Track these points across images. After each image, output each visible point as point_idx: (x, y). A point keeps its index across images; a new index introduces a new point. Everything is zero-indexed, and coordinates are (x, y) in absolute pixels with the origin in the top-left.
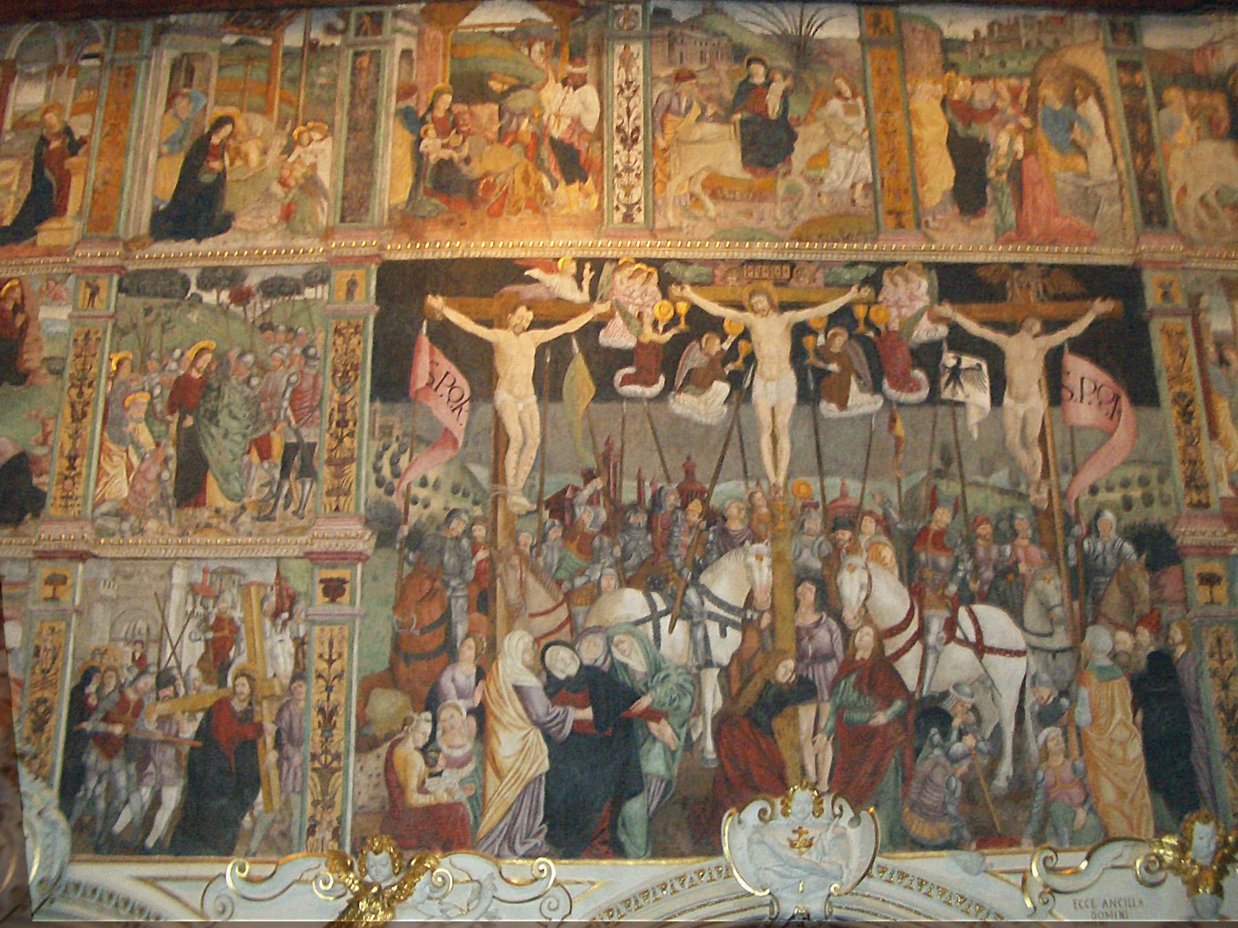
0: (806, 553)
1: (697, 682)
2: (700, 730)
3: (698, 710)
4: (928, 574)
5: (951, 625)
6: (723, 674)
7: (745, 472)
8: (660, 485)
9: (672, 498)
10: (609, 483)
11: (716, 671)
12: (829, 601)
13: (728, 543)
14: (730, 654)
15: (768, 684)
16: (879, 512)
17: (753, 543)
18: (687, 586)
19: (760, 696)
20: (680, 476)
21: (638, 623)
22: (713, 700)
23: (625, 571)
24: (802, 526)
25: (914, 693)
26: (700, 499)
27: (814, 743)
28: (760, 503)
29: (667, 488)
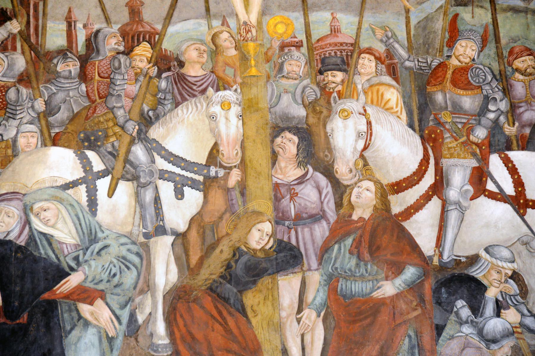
0: (286, 99)
1: (145, 253)
2: (148, 310)
3: (148, 287)
4: (446, 118)
5: (479, 177)
6: (180, 241)
7: (208, 10)
8: (96, 27)
9: (113, 41)
10: (28, 23)
11: (169, 239)
12: (314, 152)
13: (185, 90)
14: (188, 217)
15: (237, 253)
16: (381, 48)
17: (218, 90)
18: (132, 142)
19: (228, 267)
20: (122, 17)
21: (67, 186)
22: (165, 272)
23: (49, 126)
24: (281, 69)
25: (431, 258)
26: (149, 42)
27: (299, 321)
28: (227, 44)
29: (107, 30)
